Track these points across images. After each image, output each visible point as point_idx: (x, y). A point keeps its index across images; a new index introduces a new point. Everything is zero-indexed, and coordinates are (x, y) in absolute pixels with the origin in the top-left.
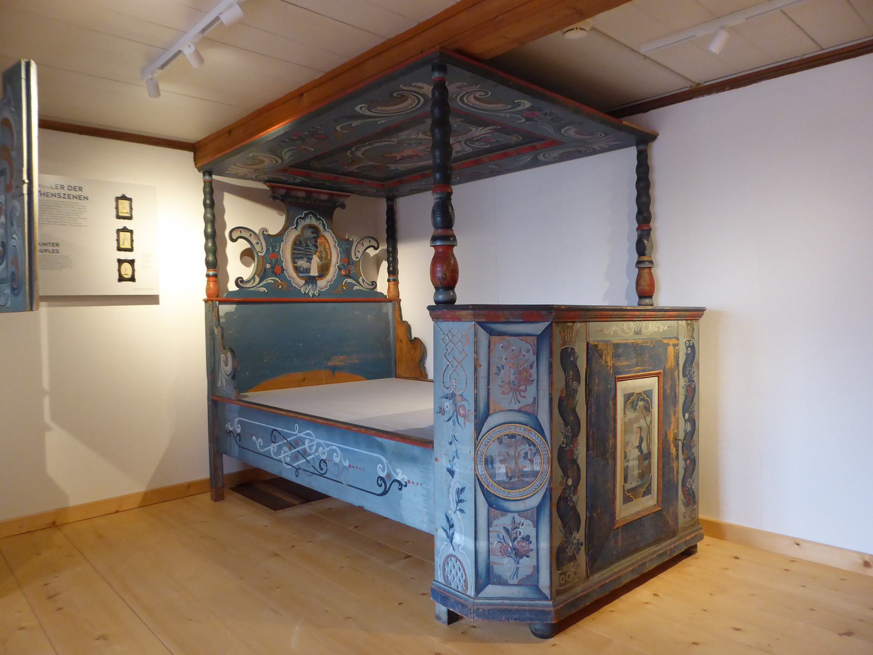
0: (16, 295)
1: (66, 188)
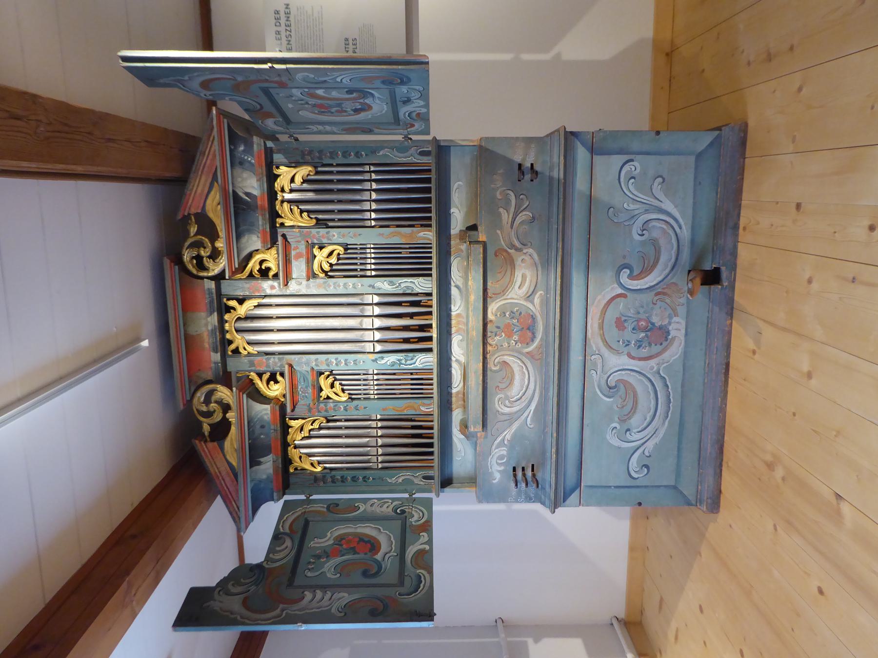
0: (409, 80)
1: (278, 29)
